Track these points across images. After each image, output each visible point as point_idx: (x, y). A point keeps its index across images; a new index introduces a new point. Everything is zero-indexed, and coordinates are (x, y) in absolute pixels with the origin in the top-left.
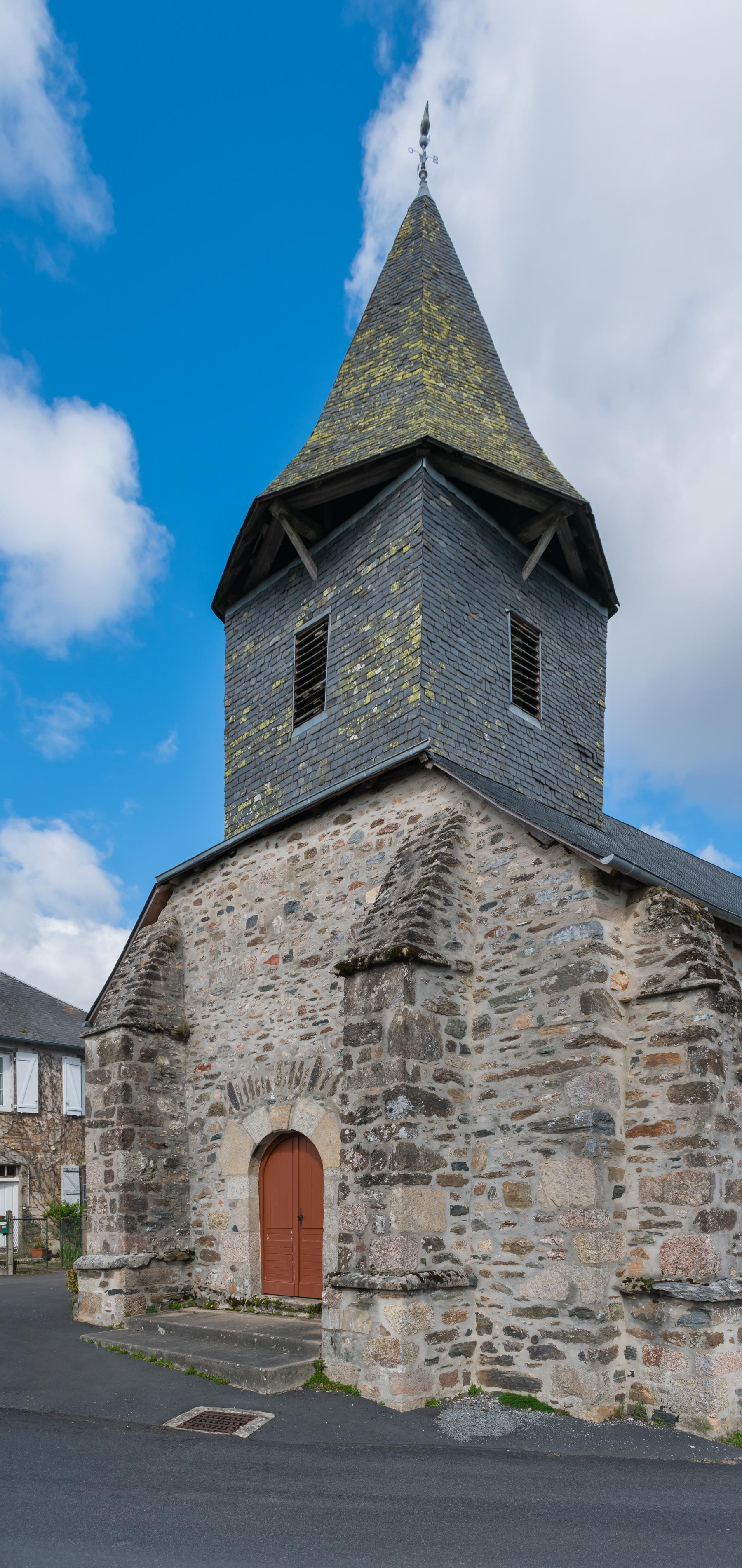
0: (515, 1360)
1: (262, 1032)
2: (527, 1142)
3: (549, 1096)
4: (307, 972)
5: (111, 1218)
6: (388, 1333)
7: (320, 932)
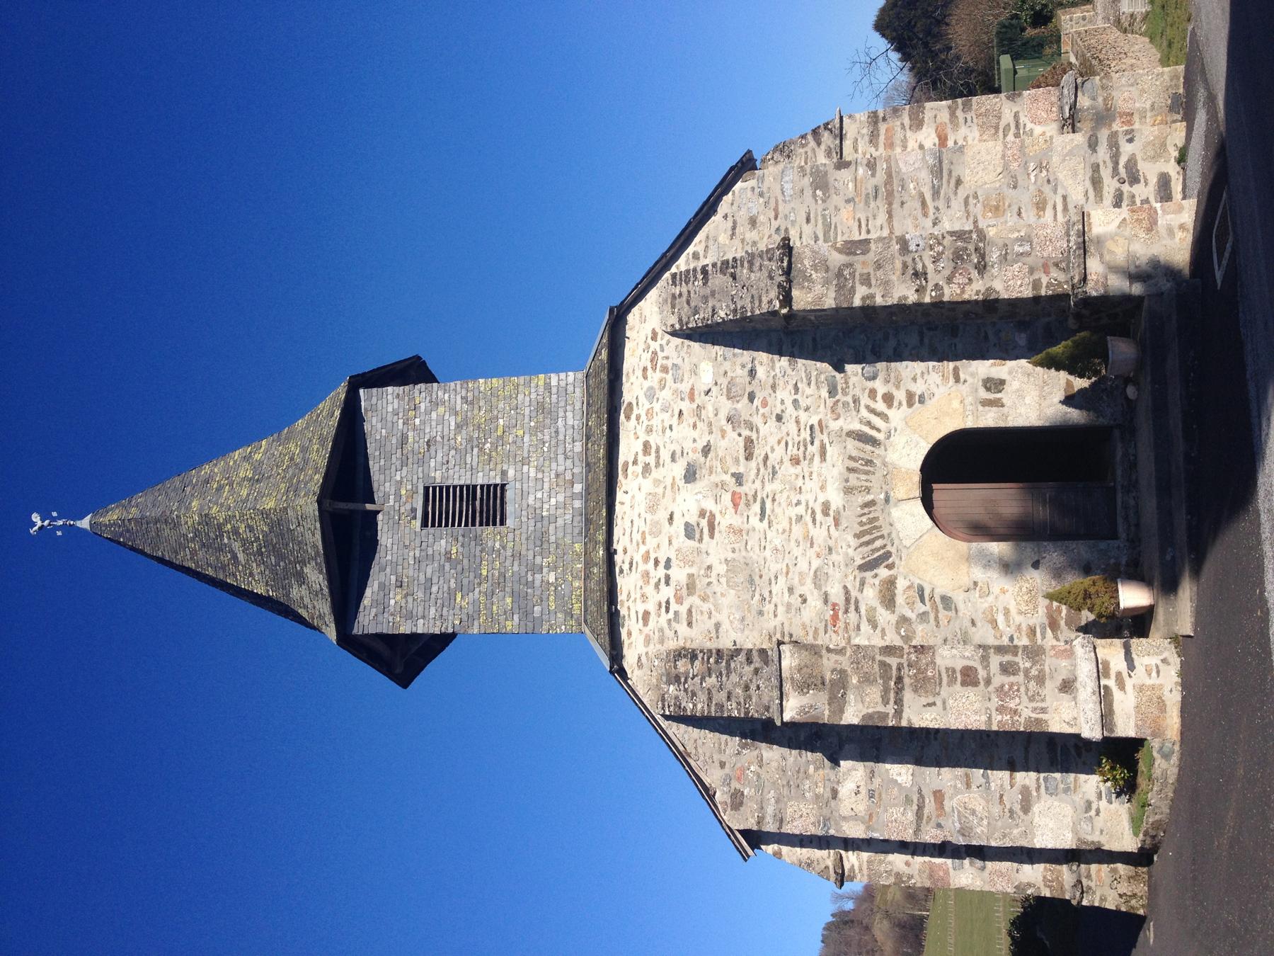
0: (1144, 197)
1: (808, 519)
2: (948, 200)
3: (912, 186)
4: (759, 452)
5: (1027, 671)
6: (1124, 219)
7: (723, 437)
